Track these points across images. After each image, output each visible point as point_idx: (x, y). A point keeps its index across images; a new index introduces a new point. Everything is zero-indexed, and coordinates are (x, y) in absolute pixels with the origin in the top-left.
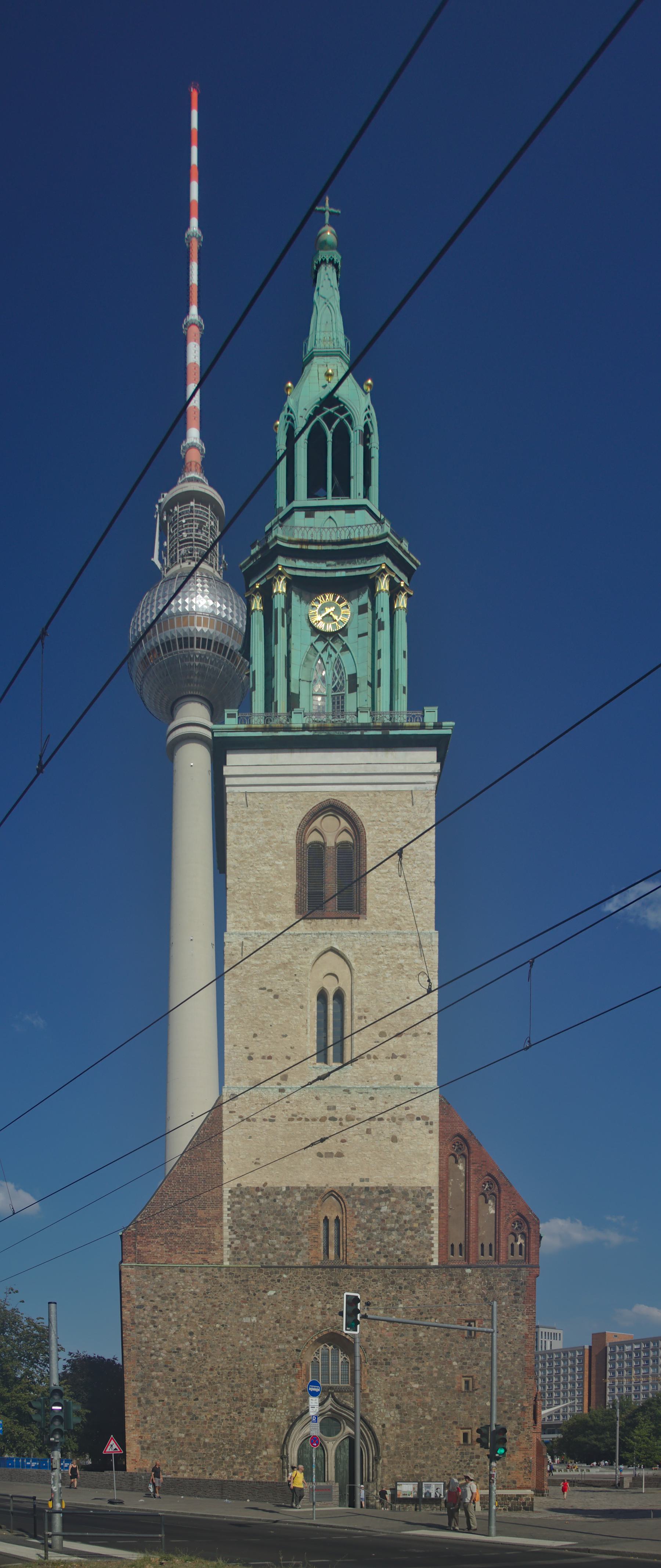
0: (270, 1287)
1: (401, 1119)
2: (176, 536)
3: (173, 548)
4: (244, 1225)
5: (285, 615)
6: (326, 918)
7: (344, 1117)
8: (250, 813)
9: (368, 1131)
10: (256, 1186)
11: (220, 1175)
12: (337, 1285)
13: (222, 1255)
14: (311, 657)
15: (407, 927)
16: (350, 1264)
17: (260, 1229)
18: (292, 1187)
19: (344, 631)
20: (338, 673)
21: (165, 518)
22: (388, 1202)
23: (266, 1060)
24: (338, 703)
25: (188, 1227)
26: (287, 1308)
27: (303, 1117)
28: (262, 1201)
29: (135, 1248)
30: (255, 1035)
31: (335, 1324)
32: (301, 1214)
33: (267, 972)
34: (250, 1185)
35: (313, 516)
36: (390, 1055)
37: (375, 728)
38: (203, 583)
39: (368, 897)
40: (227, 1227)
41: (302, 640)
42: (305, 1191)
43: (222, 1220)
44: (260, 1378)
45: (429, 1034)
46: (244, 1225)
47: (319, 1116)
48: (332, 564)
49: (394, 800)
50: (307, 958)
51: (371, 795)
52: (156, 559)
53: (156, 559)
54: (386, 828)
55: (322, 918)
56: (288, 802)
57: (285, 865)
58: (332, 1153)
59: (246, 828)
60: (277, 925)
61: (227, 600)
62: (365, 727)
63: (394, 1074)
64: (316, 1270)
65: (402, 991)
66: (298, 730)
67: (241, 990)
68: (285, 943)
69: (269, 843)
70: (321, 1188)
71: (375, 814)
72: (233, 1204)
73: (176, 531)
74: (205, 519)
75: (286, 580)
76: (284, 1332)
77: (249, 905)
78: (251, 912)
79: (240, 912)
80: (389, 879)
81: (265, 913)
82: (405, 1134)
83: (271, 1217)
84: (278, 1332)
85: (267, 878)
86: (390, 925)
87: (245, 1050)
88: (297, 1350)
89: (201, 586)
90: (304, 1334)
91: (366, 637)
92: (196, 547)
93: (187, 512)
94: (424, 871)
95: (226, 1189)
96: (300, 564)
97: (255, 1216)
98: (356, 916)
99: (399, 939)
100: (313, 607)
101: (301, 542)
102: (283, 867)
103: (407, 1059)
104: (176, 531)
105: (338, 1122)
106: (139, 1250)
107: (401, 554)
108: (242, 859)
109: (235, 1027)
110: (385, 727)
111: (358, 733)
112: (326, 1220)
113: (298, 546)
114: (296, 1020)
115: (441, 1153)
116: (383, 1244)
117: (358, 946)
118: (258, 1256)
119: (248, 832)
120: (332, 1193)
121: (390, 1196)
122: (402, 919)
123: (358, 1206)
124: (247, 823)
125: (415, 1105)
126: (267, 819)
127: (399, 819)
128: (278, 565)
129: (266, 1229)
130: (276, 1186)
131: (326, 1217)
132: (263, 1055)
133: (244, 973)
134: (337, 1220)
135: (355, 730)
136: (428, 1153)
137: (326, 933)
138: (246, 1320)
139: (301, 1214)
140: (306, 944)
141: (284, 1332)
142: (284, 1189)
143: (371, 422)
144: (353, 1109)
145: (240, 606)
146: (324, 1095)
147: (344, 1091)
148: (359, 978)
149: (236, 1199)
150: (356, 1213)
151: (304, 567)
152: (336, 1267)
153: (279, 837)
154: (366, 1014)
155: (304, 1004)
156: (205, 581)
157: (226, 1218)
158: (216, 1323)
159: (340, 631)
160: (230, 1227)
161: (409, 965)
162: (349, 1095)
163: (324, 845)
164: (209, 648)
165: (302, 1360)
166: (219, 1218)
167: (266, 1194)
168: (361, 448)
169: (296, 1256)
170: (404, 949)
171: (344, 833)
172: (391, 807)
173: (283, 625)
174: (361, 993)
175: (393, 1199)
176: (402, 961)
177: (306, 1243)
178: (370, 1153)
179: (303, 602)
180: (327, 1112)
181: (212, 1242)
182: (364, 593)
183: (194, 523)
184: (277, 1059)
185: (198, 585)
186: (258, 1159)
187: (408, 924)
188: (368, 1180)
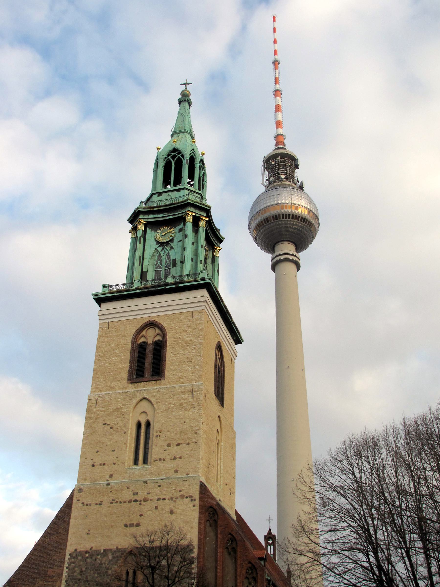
1: (176, 499)
4: (75, 579)
5: (142, 239)
6: (143, 382)
7: (142, 499)
8: (109, 332)
9: (156, 508)
11: (66, 543)
14: (155, 254)
18: (108, 549)
19: (172, 240)
20: (168, 259)
23: (102, 466)
24: (167, 273)
25: (41, 582)
27: (119, 501)
28: (88, 560)
30: (97, 452)
32: (111, 569)
33: (108, 415)
34: (83, 550)
36: (173, 457)
41: (151, 246)
42: (115, 551)
45: (196, 443)
46: (75, 579)
47: (128, 500)
48: (166, 214)
49: (183, 316)
51: (172, 316)
54: (178, 331)
55: (141, 382)
56: (129, 324)
57: (124, 356)
58: (133, 524)
59: (106, 339)
60: (117, 388)
62: (168, 284)
65: (181, 418)
66: (133, 290)
68: (119, 397)
70: (125, 548)
71: (173, 325)
72: (70, 564)
74: (286, 163)
79: (99, 383)
80: (178, 357)
81: (111, 382)
83: (92, 572)
85: (115, 363)
86: (177, 382)
87: (91, 461)
94: (198, 351)
95: (68, 553)
98: (159, 379)
99: (182, 389)
101: (150, 208)
105: (138, 503)
107: (199, 205)
108: (103, 355)
109: (87, 447)
110: (176, 283)
111: (163, 288)
113: (149, 210)
114: (121, 441)
115: (200, 522)
117: (158, 395)
122: (184, 378)
124: (107, 337)
125: (185, 488)
126: (118, 334)
127: (186, 325)
129: (88, 581)
132: (101, 463)
133: (96, 416)
135: (162, 287)
136: (192, 520)
139: (111, 569)
142: (102, 551)
144: (148, 493)
146: (132, 486)
147: (144, 482)
148: (158, 413)
149: (73, 560)
151: (152, 217)
153: (123, 342)
157: (65, 574)
160: (66, 581)
161: (186, 403)
162: (147, 484)
166: (60, 575)
170: (184, 394)
172: (181, 320)
173: (140, 243)
176: (182, 401)
179: (153, 231)
180: (133, 496)
182: (181, 223)
183: (280, 166)
184: (108, 465)
186: (89, 531)
187: (187, 380)
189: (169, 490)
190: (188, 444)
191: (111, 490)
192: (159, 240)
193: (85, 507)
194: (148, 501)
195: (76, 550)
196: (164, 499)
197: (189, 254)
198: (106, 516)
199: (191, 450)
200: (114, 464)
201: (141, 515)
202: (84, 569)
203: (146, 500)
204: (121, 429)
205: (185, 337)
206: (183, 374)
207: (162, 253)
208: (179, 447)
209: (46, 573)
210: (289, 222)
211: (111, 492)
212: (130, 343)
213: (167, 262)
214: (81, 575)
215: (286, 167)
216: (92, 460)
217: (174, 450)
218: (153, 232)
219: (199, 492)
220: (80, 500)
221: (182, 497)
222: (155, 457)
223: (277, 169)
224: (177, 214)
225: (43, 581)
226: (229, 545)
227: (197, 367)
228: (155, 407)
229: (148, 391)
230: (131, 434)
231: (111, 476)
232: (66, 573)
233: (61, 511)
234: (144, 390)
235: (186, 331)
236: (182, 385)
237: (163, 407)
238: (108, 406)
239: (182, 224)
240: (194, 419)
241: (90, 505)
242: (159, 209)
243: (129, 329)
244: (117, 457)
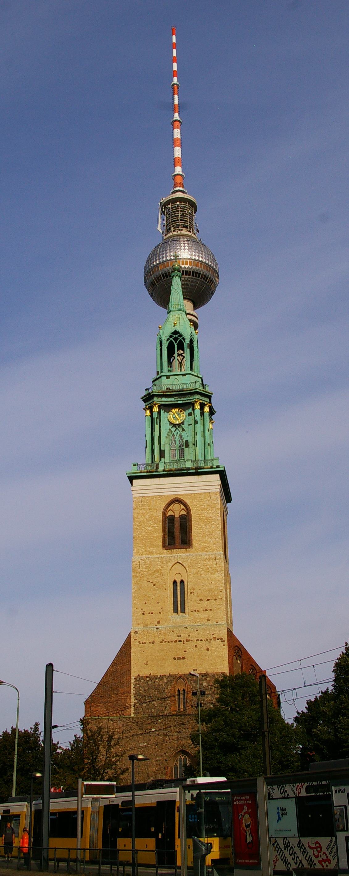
0: (153, 727)
1: (211, 640)
2: (170, 218)
3: (168, 225)
5: (158, 420)
8: (143, 505)
9: (196, 646)
10: (146, 675)
11: (130, 671)
12: (183, 724)
13: (131, 711)
14: (169, 434)
15: (210, 551)
16: (190, 713)
17: (148, 697)
18: (162, 675)
19: (183, 423)
20: (181, 440)
21: (163, 210)
22: (206, 681)
23: (150, 615)
24: (181, 452)
26: (161, 737)
28: (149, 682)
29: (91, 709)
31: (183, 745)
32: (167, 688)
33: (150, 574)
35: (167, 389)
36: (205, 610)
37: (192, 469)
38: (184, 244)
39: (193, 539)
40: (133, 697)
41: (166, 428)
42: (168, 677)
43: (131, 693)
44: (149, 776)
45: (221, 599)
47: (174, 640)
49: (202, 496)
50: (167, 567)
52: (159, 229)
53: (159, 229)
55: (174, 549)
56: (158, 500)
57: (158, 526)
58: (180, 658)
59: (141, 511)
61: (199, 250)
62: (189, 469)
63: (207, 618)
64: (174, 717)
66: (161, 472)
67: (139, 583)
69: (151, 517)
71: (195, 503)
72: (136, 685)
73: (170, 216)
75: (158, 406)
76: (159, 751)
77: (143, 544)
78: (143, 547)
79: (139, 548)
81: (149, 548)
82: (212, 647)
83: (153, 690)
84: (157, 750)
85: (150, 532)
86: (203, 550)
88: (166, 760)
89: (183, 245)
90: (169, 751)
91: (191, 426)
92: (180, 224)
93: (176, 207)
95: (133, 678)
96: (164, 399)
97: (146, 690)
99: (207, 557)
100: (170, 414)
102: (157, 528)
103: (212, 611)
104: (170, 216)
105: (182, 642)
106: (92, 710)
108: (139, 525)
110: (197, 468)
111: (186, 471)
112: (179, 691)
113: (162, 394)
114: (163, 595)
116: (204, 702)
117: (189, 561)
118: (147, 711)
119: (142, 513)
120: (180, 677)
121: (207, 678)
122: (208, 547)
123: (193, 683)
124: (141, 509)
127: (204, 505)
128: (154, 401)
129: (151, 697)
130: (155, 675)
131: (179, 689)
134: (184, 690)
137: (175, 556)
138: (142, 745)
139: (167, 688)
140: (167, 561)
141: (159, 751)
142: (159, 676)
143: (193, 338)
144: (189, 636)
145: (206, 252)
147: (185, 627)
148: (190, 575)
149: (137, 682)
150: (192, 687)
152: (183, 715)
153: (155, 515)
154: (193, 591)
155: (167, 588)
156: (186, 242)
157: (133, 692)
158: (127, 747)
159: (181, 423)
160: (134, 697)
163: (174, 516)
164: (189, 275)
165: (168, 765)
166: (130, 692)
167: (151, 679)
168: (189, 350)
169: (165, 710)
171: (183, 510)
172: (201, 500)
173: (157, 424)
174: (191, 582)
175: (208, 679)
176: (208, 566)
177: (169, 703)
178: (197, 656)
179: (166, 412)
180: (177, 637)
181: (126, 705)
182: (190, 408)
183: (179, 212)
184: (155, 614)
185: (181, 245)
188: (196, 670)
189: (205, 633)
190: (216, 600)
191: (160, 633)
192: (172, 422)
193: (141, 644)
194: (189, 641)
195: (139, 675)
196: (201, 640)
197: (199, 438)
198: (158, 651)
199: (218, 605)
200: (160, 613)
201: (185, 651)
202: (147, 689)
203: (187, 641)
204: (162, 586)
205: (205, 514)
206: (206, 544)
207: (175, 433)
208: (209, 601)
209: (118, 691)
210: (189, 279)
211: (160, 634)
212: (161, 516)
213: (180, 442)
214: (145, 692)
215: (185, 214)
216: (142, 609)
217: (205, 604)
218: (166, 413)
219: (227, 636)
220: (136, 640)
221: (215, 639)
222: (191, 609)
223: (176, 216)
224: (186, 400)
225: (117, 696)
226: (250, 672)
227: (217, 539)
228: (187, 570)
229: (181, 558)
230: (170, 590)
231: (159, 622)
232: (134, 691)
233: (122, 648)
234: (178, 556)
235: (206, 509)
236: (207, 553)
237: (194, 570)
238: (149, 568)
239: (191, 409)
240: (218, 581)
241: (145, 643)
242: (171, 393)
243: (159, 504)
244: (162, 608)
